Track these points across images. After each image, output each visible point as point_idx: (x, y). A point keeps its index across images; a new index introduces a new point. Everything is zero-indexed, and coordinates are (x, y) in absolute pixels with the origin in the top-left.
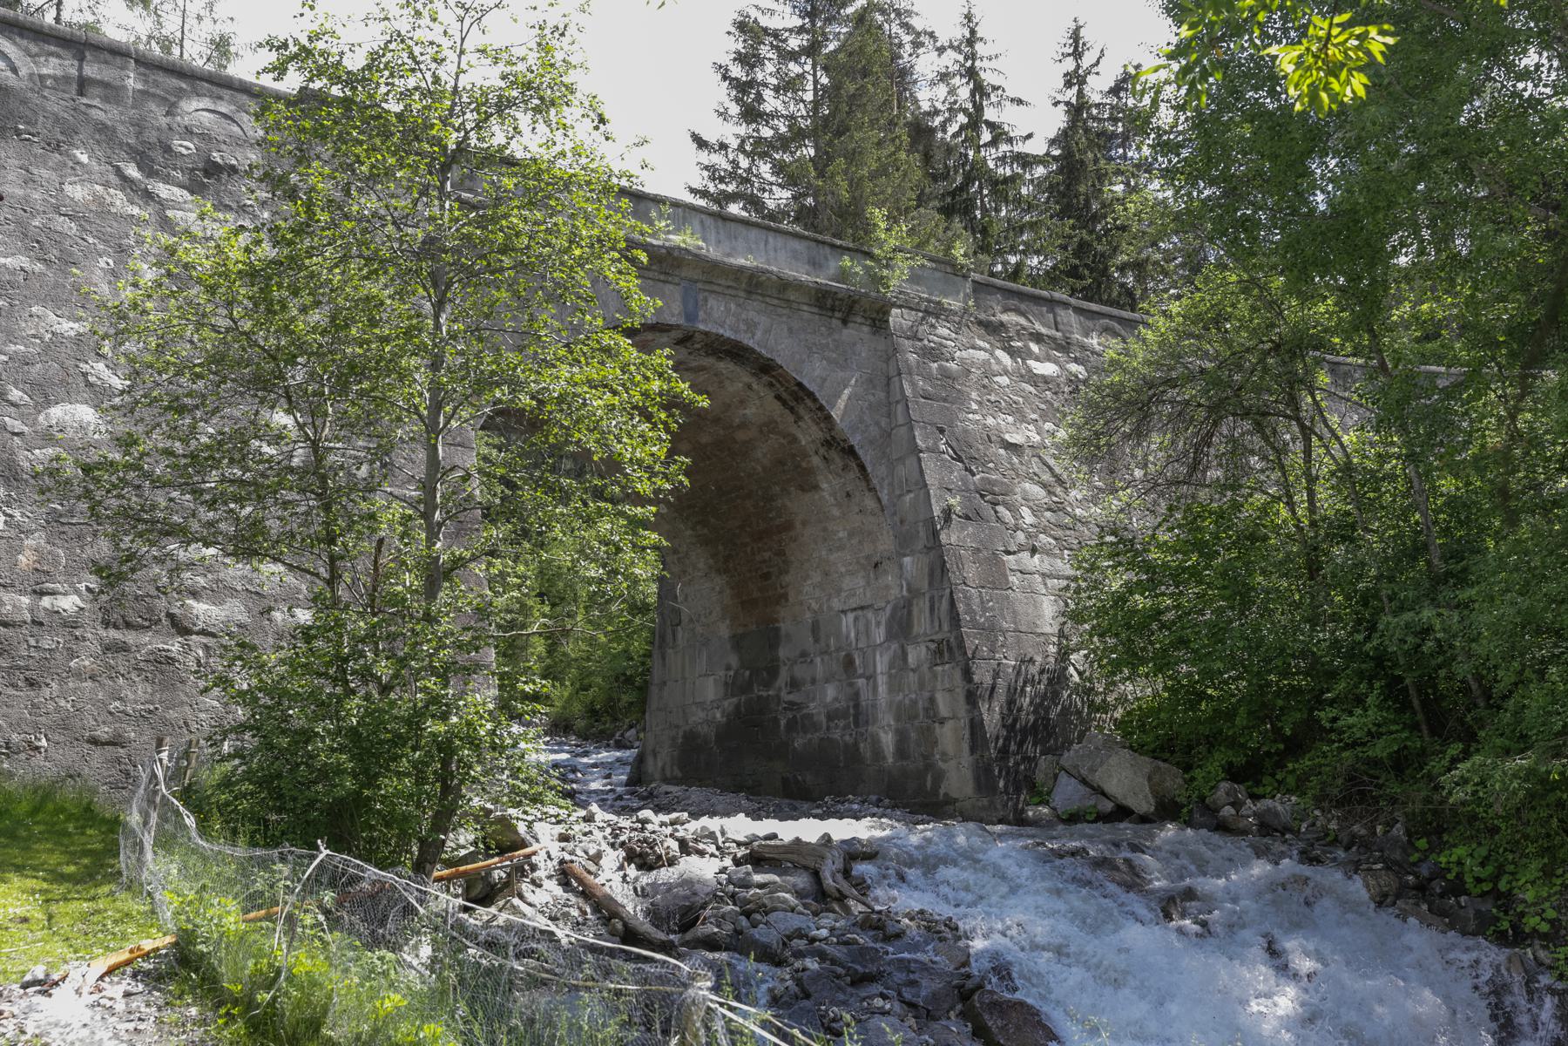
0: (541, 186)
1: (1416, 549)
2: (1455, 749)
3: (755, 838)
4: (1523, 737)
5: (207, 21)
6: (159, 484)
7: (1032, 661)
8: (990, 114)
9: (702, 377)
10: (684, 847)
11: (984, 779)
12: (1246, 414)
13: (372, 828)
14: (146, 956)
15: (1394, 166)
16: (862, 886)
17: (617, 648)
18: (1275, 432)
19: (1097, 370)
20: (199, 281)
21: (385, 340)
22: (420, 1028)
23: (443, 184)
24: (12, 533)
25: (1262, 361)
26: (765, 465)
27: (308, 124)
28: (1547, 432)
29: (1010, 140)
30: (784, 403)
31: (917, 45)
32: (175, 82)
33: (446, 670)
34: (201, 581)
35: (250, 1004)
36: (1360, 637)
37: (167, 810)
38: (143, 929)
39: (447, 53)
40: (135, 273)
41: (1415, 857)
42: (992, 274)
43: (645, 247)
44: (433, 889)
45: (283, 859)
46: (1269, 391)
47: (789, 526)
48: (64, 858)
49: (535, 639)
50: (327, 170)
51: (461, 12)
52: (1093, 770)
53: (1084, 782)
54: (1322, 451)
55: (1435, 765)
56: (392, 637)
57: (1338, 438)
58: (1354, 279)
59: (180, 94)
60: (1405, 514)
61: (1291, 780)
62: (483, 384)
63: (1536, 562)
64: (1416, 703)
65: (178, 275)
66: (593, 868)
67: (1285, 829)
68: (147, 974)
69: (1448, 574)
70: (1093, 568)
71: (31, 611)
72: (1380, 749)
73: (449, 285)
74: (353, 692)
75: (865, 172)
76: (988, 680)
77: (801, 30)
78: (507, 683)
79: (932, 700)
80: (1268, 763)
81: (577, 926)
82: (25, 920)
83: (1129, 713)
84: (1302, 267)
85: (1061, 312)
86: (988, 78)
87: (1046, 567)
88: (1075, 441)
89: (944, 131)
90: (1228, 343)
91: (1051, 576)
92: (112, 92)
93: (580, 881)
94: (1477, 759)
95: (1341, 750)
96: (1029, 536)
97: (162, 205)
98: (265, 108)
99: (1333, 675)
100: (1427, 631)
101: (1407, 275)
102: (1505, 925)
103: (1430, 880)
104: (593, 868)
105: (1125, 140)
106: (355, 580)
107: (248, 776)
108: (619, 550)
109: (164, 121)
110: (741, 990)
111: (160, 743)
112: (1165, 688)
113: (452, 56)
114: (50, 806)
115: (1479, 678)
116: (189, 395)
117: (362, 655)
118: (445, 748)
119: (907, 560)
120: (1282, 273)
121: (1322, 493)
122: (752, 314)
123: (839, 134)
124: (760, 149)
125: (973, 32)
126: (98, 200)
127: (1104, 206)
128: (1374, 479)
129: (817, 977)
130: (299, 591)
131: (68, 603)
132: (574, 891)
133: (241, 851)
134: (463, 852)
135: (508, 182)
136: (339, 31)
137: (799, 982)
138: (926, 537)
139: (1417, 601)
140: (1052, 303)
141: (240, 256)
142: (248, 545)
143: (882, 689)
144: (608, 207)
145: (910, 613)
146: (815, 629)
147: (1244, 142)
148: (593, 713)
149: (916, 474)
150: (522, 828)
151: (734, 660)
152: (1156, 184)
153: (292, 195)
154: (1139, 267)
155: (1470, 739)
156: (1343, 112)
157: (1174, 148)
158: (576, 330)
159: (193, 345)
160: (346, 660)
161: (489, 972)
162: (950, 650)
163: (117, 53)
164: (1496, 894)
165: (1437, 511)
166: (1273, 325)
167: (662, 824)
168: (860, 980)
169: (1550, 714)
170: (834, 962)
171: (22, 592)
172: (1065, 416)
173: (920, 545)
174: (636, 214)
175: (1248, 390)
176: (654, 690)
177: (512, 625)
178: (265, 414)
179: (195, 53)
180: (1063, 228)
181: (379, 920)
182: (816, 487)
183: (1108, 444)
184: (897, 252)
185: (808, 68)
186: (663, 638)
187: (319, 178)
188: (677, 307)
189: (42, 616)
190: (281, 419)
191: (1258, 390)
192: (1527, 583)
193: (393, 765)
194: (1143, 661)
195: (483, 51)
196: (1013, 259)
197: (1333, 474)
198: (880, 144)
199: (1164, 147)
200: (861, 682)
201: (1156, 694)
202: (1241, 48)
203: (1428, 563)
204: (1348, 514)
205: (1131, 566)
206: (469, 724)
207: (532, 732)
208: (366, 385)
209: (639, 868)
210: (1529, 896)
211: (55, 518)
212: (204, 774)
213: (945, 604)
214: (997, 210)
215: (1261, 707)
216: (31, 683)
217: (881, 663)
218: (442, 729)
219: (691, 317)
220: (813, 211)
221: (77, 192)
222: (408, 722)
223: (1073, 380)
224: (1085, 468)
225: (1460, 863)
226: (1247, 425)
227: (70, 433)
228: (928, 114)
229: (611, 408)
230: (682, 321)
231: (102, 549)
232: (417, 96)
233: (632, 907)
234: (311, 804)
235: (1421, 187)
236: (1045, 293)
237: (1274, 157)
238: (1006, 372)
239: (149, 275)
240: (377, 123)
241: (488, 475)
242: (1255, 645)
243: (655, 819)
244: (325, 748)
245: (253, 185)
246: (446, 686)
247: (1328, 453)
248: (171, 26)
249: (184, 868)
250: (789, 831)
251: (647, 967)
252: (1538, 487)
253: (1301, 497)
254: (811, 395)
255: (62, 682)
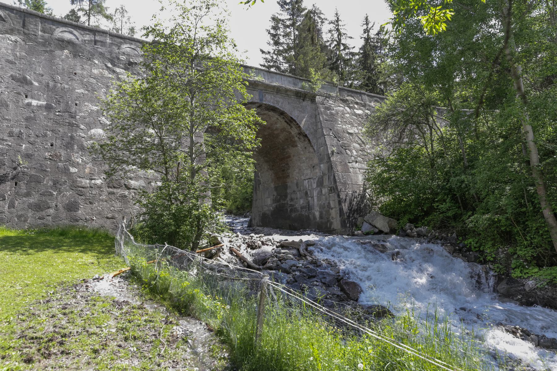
0: (219, 64)
1: (460, 159)
2: (470, 213)
3: (282, 240)
4: (488, 209)
5: (128, 23)
6: (120, 149)
7: (356, 192)
8: (343, 41)
9: (265, 116)
10: (263, 243)
11: (343, 224)
12: (414, 123)
13: (180, 239)
14: (123, 272)
15: (455, 53)
16: (311, 253)
17: (244, 191)
18: (422, 128)
19: (373, 112)
20: (128, 95)
21: (178, 108)
22: (193, 290)
23: (192, 65)
24: (83, 164)
25: (419, 108)
26: (279, 144)
27: (155, 50)
28: (496, 127)
29: (349, 49)
30: (287, 123)
31: (322, 22)
32: (120, 40)
33: (198, 197)
34: (132, 175)
35: (150, 284)
36: (445, 184)
37: (127, 236)
38: (122, 266)
39: (192, 28)
40: (111, 92)
41: (459, 242)
42: (344, 86)
43: (248, 81)
44: (196, 255)
45: (156, 248)
46: (421, 117)
47: (289, 157)
48: (101, 248)
49: (222, 189)
50: (160, 62)
51: (195, 17)
52: (373, 221)
53: (370, 224)
54: (435, 133)
55: (464, 217)
56: (183, 189)
57: (439, 130)
58: (444, 85)
59: (121, 43)
60: (457, 150)
61: (426, 223)
62: (205, 120)
63: (493, 162)
64: (460, 201)
65: (122, 93)
66: (239, 249)
67: (424, 236)
68: (124, 277)
69: (469, 166)
70: (373, 166)
71: (89, 184)
72: (450, 214)
73: (195, 93)
74: (173, 204)
75: (308, 58)
76: (344, 197)
77: (290, 19)
78: (214, 200)
79: (329, 203)
80: (420, 218)
81: (235, 264)
82: (93, 263)
83: (382, 206)
84: (429, 82)
85: (363, 96)
86: (342, 31)
87: (360, 167)
88: (367, 132)
89: (330, 46)
90: (409, 104)
91: (361, 169)
92: (103, 44)
93: (235, 253)
94: (476, 215)
95: (439, 214)
96: (355, 158)
97: (118, 74)
98: (144, 46)
99: (437, 194)
100: (463, 182)
101: (458, 84)
102: (482, 259)
103: (462, 248)
104: (239, 249)
105: (381, 48)
106: (173, 174)
107: (147, 226)
108: (243, 164)
109: (117, 51)
110: (277, 279)
111: (123, 218)
112: (392, 199)
113: (193, 29)
114: (97, 235)
115: (477, 194)
116: (126, 125)
117: (175, 194)
118: (198, 218)
119: (322, 165)
120: (424, 84)
121: (435, 145)
122: (278, 99)
123: (301, 48)
124: (279, 53)
125: (338, 18)
126: (101, 73)
127: (375, 66)
128: (449, 140)
129: (299, 276)
130: (158, 177)
131: (99, 182)
132: (234, 255)
133: (146, 246)
134: (204, 245)
135: (210, 64)
136: (163, 24)
137: (294, 278)
138: (327, 159)
139: (460, 173)
140: (361, 94)
141: (138, 87)
142: (144, 165)
143: (316, 200)
144: (238, 70)
145: (323, 180)
146: (297, 184)
147: (414, 46)
148: (238, 208)
149: (324, 142)
150: (219, 239)
151: (275, 193)
152: (389, 60)
153: (151, 69)
154: (385, 83)
155: (474, 210)
156: (440, 36)
157: (394, 49)
158: (230, 104)
159: (127, 112)
160: (171, 195)
161: (211, 276)
162: (334, 189)
163: (104, 33)
164: (479, 251)
165: (466, 149)
166: (422, 99)
167: (257, 237)
168: (310, 277)
169: (495, 203)
170: (303, 273)
171: (87, 179)
172: (365, 124)
173: (325, 161)
174: (245, 72)
175: (414, 117)
176: (254, 202)
177: (215, 185)
178: (147, 129)
179: (125, 32)
180: (365, 73)
181: (183, 263)
182: (296, 146)
183: (377, 132)
184: (317, 80)
185: (292, 30)
186: (256, 188)
187: (158, 65)
188: (257, 97)
189: (92, 185)
190: (151, 131)
191: (417, 116)
192: (490, 168)
193: (185, 223)
194: (386, 191)
195: (202, 28)
196: (350, 82)
197: (438, 139)
198: (312, 51)
199: (392, 49)
200: (310, 199)
201: (390, 200)
202: (413, 20)
203: (464, 163)
204: (442, 150)
205: (383, 165)
206: (204, 211)
207: (221, 214)
208: (173, 121)
209: (251, 249)
210: (488, 251)
211: (94, 159)
212: (136, 226)
213: (332, 177)
214: (345, 68)
215: (418, 203)
216: (91, 203)
217: (315, 193)
218: (197, 213)
219: (261, 100)
220: (294, 70)
221: (95, 71)
222: (188, 211)
223: (367, 115)
224: (370, 139)
225: (470, 243)
226: (415, 126)
227: (97, 137)
228: (326, 42)
229: (240, 125)
230: (259, 101)
231: (106, 167)
232: (184, 41)
233: (250, 259)
234: (164, 233)
235: (462, 59)
236: (359, 91)
237: (422, 51)
238: (348, 113)
239: (115, 93)
240: (174, 49)
241: (207, 145)
242: (416, 187)
243: (255, 236)
244: (166, 219)
245: (141, 67)
246: (198, 201)
247: (437, 133)
248: (118, 25)
249: (132, 250)
250: (290, 239)
251: (252, 274)
252: (493, 142)
253: (429, 146)
254: (295, 121)
255: (98, 202)
